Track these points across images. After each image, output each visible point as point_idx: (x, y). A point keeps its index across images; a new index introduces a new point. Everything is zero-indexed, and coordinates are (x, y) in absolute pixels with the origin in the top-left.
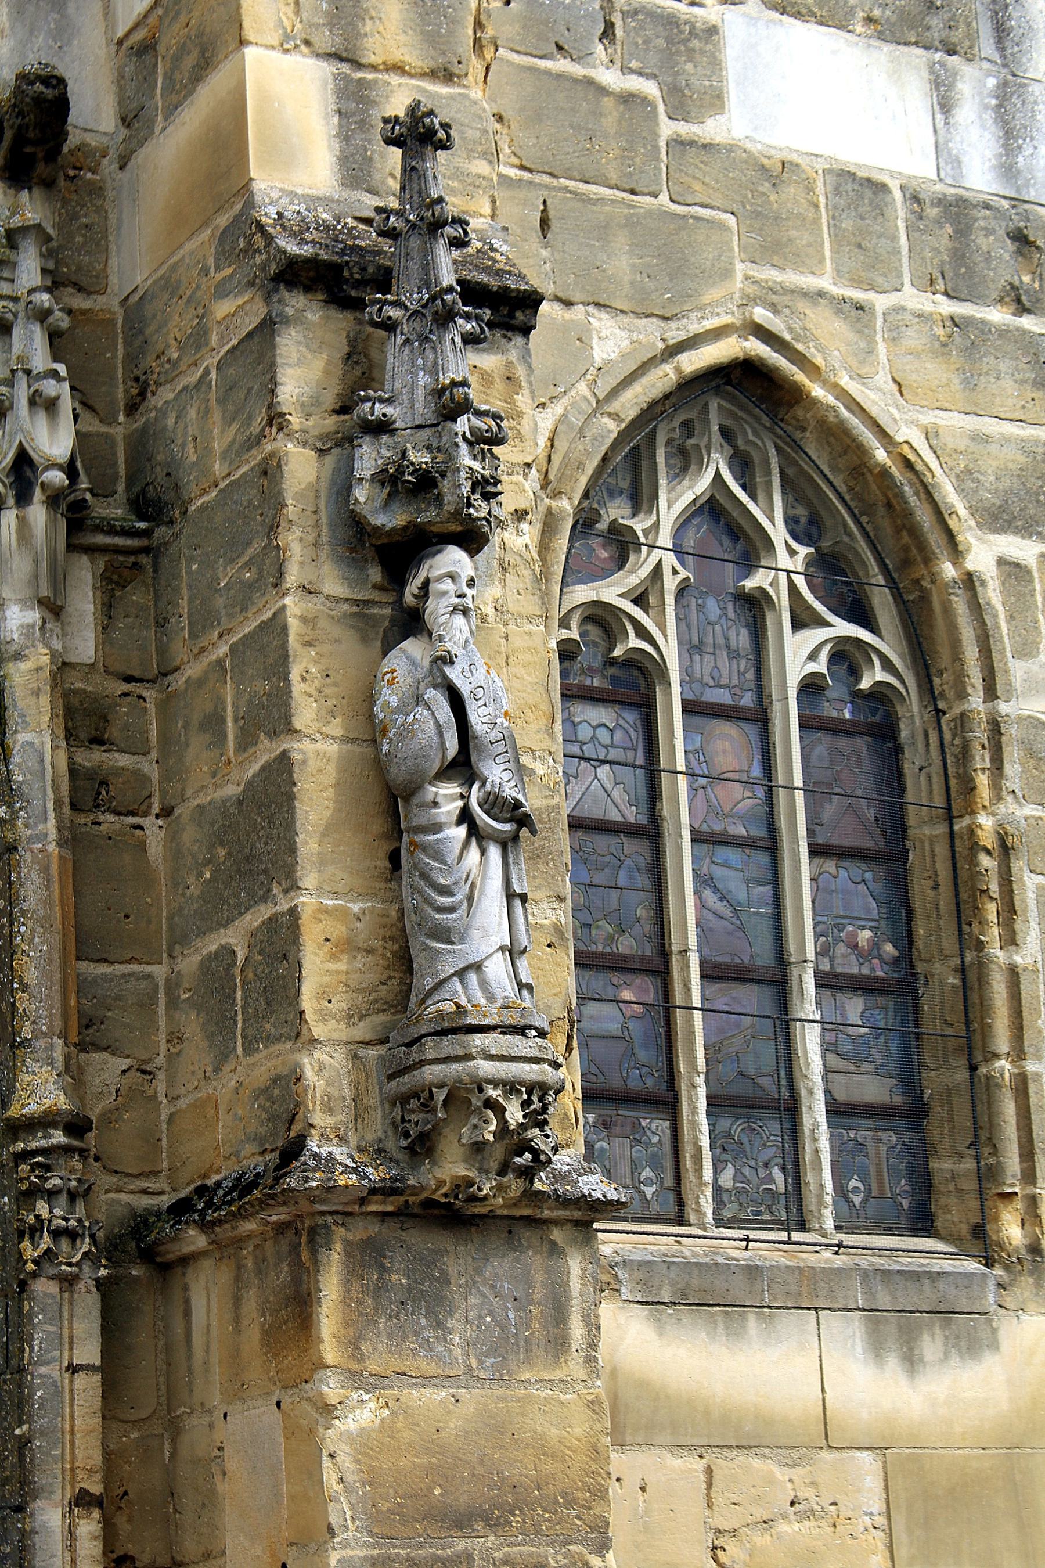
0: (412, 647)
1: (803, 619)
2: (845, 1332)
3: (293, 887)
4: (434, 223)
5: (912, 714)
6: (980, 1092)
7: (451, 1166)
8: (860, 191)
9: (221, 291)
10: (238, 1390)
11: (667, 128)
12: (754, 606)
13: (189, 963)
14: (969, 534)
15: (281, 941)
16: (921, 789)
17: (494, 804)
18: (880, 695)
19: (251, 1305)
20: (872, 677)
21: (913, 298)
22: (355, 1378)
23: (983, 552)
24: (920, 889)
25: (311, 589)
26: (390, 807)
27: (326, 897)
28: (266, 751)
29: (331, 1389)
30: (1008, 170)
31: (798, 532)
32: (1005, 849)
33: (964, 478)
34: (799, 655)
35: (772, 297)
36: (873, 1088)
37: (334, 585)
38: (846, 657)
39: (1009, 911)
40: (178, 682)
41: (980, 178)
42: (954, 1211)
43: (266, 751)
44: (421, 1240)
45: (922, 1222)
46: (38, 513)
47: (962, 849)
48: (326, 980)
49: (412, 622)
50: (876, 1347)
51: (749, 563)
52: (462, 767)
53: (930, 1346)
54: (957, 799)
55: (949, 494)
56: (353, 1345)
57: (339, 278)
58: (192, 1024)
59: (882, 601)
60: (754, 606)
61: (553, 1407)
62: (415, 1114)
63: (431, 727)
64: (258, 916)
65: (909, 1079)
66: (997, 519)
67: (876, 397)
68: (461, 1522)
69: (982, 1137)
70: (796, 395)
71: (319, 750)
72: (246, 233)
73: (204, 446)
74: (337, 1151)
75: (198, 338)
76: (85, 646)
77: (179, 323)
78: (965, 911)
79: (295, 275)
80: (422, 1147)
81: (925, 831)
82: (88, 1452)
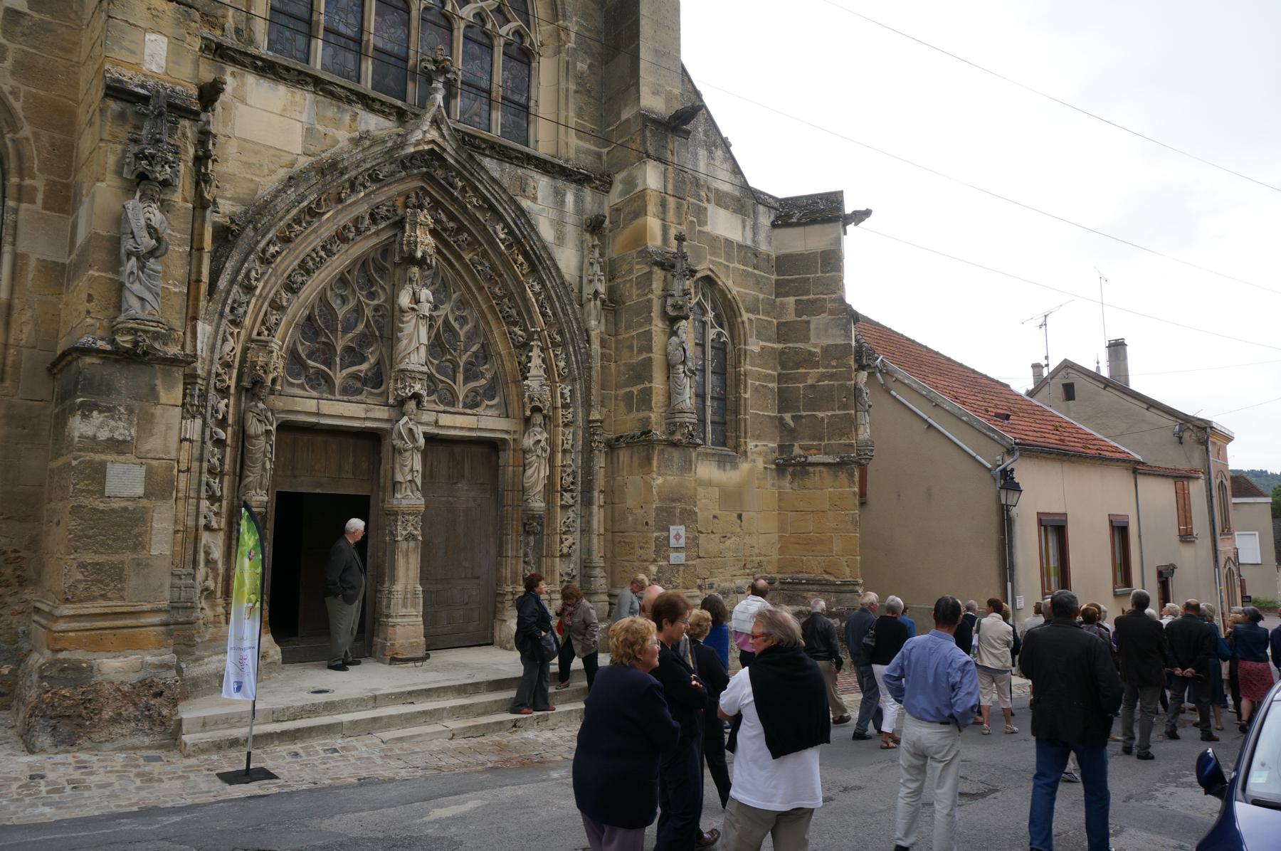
0: (674, 338)
1: (713, 327)
2: (714, 464)
3: (650, 382)
4: (684, 257)
5: (730, 347)
6: (738, 422)
7: (678, 437)
8: (729, 242)
9: (638, 263)
10: (631, 473)
11: (698, 228)
12: (704, 323)
13: (622, 392)
14: (743, 312)
15: (648, 393)
16: (730, 360)
17: (690, 370)
18: (724, 343)
19: (635, 458)
20: (723, 339)
21: (737, 265)
22: (659, 474)
23: (746, 316)
24: (729, 381)
25: (658, 326)
26: (670, 367)
27: (658, 384)
28: (645, 355)
29: (655, 476)
30: (754, 241)
31: (713, 310)
32: (745, 375)
33: (743, 302)
34: (711, 334)
35: (713, 262)
36: (717, 419)
37: (660, 325)
38: (719, 335)
39: (746, 386)
40: (620, 337)
41: (749, 243)
42: (731, 443)
43: (645, 355)
44: (670, 449)
45: (724, 445)
46: (598, 302)
47: (738, 375)
48: (658, 398)
49: (675, 333)
50: (719, 467)
51: (703, 315)
52: (684, 363)
53: (728, 467)
54: (738, 363)
55: (740, 305)
56: (659, 468)
57: (667, 265)
58: (622, 404)
59: (726, 325)
60: (704, 323)
61: (689, 480)
62: (672, 427)
63: (679, 355)
64: (640, 387)
65: (723, 418)
66: (748, 311)
67: (730, 283)
68: (674, 501)
69: (737, 429)
70: (716, 283)
71: (657, 356)
72: (645, 254)
73: (632, 295)
74: (658, 433)
75: (631, 271)
76: (603, 329)
77: (625, 267)
78: (737, 386)
79: (657, 264)
80: (672, 433)
81: (730, 370)
82: (602, 483)
